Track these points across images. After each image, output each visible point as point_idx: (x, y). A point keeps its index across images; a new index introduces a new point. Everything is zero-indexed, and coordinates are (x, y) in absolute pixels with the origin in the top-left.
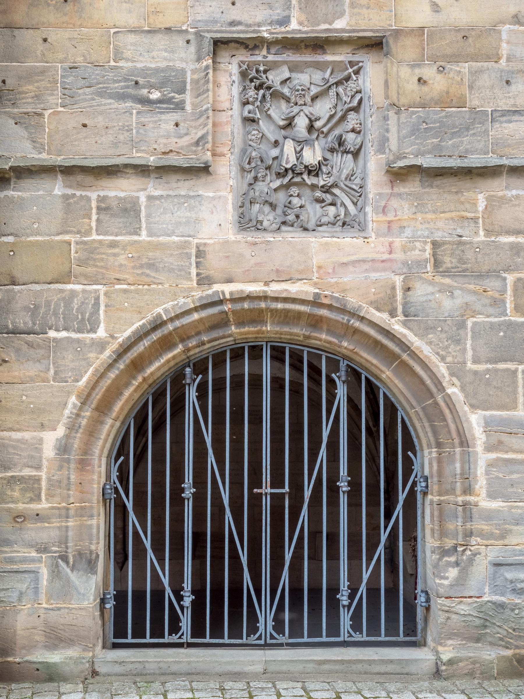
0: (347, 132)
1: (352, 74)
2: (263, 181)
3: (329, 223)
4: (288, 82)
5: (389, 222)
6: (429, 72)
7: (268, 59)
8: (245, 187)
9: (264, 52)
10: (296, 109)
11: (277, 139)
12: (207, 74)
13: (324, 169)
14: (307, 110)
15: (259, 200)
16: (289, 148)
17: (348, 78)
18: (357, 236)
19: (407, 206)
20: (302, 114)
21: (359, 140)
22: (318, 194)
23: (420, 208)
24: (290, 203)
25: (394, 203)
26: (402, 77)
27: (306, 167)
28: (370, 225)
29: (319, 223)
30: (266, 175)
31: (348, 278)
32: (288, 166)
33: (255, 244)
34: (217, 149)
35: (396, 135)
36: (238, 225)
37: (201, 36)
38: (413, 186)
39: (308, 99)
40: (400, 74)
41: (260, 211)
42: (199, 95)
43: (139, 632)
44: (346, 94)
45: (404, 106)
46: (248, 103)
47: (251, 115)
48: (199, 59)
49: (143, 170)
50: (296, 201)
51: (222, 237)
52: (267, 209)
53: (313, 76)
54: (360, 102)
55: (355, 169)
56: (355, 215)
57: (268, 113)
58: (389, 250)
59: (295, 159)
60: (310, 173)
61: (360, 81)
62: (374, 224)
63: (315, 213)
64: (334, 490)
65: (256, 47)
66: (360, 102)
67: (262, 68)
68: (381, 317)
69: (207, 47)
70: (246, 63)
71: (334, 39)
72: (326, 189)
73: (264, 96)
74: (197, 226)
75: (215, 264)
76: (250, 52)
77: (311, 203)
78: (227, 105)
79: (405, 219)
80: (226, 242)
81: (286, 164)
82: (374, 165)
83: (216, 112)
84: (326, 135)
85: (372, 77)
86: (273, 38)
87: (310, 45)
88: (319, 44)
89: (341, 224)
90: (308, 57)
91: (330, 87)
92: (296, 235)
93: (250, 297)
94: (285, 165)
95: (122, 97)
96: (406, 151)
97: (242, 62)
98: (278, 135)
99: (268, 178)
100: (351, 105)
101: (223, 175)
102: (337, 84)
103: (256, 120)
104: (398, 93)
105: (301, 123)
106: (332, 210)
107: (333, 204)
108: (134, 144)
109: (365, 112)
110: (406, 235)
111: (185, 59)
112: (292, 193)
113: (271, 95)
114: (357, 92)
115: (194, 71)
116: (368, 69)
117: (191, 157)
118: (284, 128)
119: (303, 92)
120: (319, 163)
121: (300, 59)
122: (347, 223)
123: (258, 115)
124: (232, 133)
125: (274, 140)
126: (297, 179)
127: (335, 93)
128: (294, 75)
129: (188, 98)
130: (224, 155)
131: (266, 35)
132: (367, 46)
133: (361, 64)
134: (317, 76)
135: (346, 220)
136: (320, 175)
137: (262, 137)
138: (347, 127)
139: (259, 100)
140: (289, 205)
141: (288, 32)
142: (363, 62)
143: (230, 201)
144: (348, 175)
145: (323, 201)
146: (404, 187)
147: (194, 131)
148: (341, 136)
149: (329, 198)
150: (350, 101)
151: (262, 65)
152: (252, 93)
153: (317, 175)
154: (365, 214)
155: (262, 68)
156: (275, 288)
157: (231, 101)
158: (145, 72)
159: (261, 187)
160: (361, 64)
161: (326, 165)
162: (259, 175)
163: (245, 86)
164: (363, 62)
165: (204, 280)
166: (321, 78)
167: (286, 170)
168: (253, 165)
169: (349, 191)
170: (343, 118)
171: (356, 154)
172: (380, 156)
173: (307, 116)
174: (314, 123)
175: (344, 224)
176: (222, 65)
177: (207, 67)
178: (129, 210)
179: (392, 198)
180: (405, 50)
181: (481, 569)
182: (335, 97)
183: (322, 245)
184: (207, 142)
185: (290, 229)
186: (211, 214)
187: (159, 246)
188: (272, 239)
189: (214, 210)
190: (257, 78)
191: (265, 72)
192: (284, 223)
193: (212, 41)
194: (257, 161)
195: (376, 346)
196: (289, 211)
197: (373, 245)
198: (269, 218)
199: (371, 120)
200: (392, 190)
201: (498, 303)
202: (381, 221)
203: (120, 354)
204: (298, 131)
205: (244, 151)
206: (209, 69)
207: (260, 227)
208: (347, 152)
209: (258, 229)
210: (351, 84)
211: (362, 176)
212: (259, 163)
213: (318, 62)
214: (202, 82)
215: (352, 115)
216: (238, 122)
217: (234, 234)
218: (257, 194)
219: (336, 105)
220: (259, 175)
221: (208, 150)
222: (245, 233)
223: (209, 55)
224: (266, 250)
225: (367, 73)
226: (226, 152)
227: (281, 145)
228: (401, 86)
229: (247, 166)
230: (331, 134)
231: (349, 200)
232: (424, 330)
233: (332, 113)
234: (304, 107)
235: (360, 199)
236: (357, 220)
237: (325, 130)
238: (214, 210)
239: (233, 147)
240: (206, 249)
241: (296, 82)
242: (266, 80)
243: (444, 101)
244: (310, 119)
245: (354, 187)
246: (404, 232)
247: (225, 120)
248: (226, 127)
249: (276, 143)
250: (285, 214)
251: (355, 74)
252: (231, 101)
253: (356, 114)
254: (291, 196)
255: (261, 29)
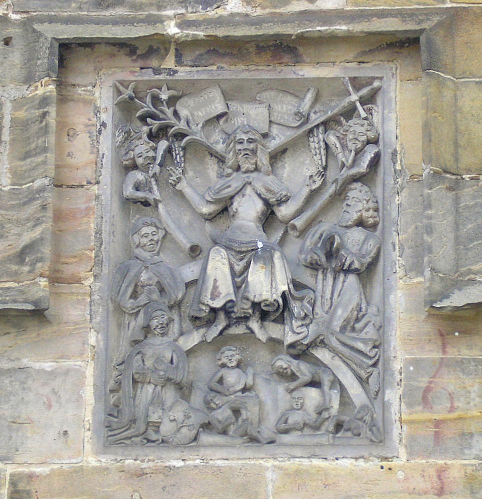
0: (347, 227)
1: (358, 104)
2: (163, 335)
3: (305, 425)
4: (222, 121)
5: (438, 423)
7: (177, 77)
8: (125, 347)
9: (170, 62)
10: (236, 181)
11: (196, 242)
12: (45, 114)
13: (296, 307)
14: (261, 181)
15: (153, 378)
17: (350, 113)
18: (366, 455)
19: (476, 387)
20: (249, 190)
21: (371, 247)
22: (284, 362)
24: (221, 381)
25: (449, 381)
26: (466, 109)
27: (256, 305)
28: (396, 431)
29: (283, 426)
30: (171, 320)
32: (217, 304)
33: (141, 474)
34: (65, 268)
35: (451, 236)
36: (104, 432)
37: (34, 31)
39: (263, 160)
40: (460, 103)
41: (157, 401)
42: (27, 155)
44: (344, 147)
45: (469, 171)
46: (135, 167)
47: (140, 195)
48: (29, 80)
50: (233, 378)
51: (66, 462)
52: (170, 395)
53: (277, 107)
54: (376, 162)
55: (364, 306)
56: (364, 407)
57: (178, 187)
58: (436, 483)
59: (232, 290)
60: (264, 316)
61: (376, 118)
62: (405, 428)
63: (275, 401)
65: (151, 51)
66: (376, 162)
67: (164, 97)
69: (45, 58)
70: (132, 86)
71: (316, 35)
72: (301, 352)
73: (169, 151)
74: (14, 435)
76: (140, 63)
77: (267, 381)
78: (89, 173)
79: (472, 418)
80: (79, 471)
81: (212, 299)
82: (401, 296)
83: (64, 189)
84: (303, 233)
86: (187, 36)
87: (269, 47)
89: (331, 428)
90: (264, 72)
91: (311, 131)
92: (233, 453)
94: (210, 303)
96: (475, 268)
97: (122, 83)
98: (201, 234)
99: (175, 328)
100: (354, 171)
101: (75, 323)
102: (326, 125)
103: (152, 202)
104: (456, 145)
105: (248, 209)
106: (312, 395)
107: (314, 383)
109: (384, 185)
110: (475, 451)
112: (224, 360)
113: (184, 149)
114: (368, 142)
115: (18, 103)
116: (392, 95)
117: (7, 285)
118: (211, 218)
119: (252, 146)
120: (284, 295)
121: (245, 75)
122: (345, 426)
123: (157, 195)
124: (99, 232)
125: (188, 246)
126: (239, 330)
127: (322, 144)
128: (234, 106)
130: (79, 281)
131: (172, 29)
132: (390, 45)
133: (376, 84)
134: (285, 108)
135: (346, 418)
136: (287, 321)
137: (164, 237)
138: (347, 216)
139: (158, 161)
140: (218, 387)
141: (220, 22)
142: (381, 78)
143: (90, 381)
144: (347, 321)
145: (293, 377)
146: (470, 347)
147: (15, 230)
148: (330, 240)
149: (304, 370)
150: (354, 161)
151: (164, 88)
152: (142, 148)
153: (281, 320)
154: (385, 406)
155: (164, 97)
157: (97, 165)
159: (159, 348)
160: (376, 84)
161: (301, 299)
162: (154, 323)
163: (128, 133)
164: (381, 78)
166: (295, 110)
167: (213, 310)
168: (143, 299)
169: (349, 354)
170: (340, 195)
171: (367, 273)
172: (415, 281)
173: (259, 195)
174: (276, 209)
175: (339, 427)
176: (80, 90)
177: (44, 101)
179: (444, 370)
182: (323, 152)
183: (288, 475)
184: (41, 260)
185: (219, 439)
188: (180, 464)
189: (53, 399)
190: (154, 117)
191: (172, 101)
192: (207, 426)
193: (57, 45)
194: (150, 292)
196: (218, 400)
197: (401, 475)
198: (174, 416)
199: (399, 201)
200: (444, 352)
202: (419, 422)
204: (239, 228)
205: (123, 271)
206: (47, 105)
207: (154, 437)
208: (348, 271)
209: (149, 441)
210: (357, 129)
211: (378, 320)
212: (155, 296)
213: (284, 81)
214: (35, 128)
215: (357, 192)
216: (115, 207)
217: (97, 453)
218: (149, 363)
219: (325, 168)
220: (154, 323)
221: (41, 276)
222: (120, 450)
223: (48, 76)
224: (164, 488)
225: (390, 101)
226: (82, 274)
227: (204, 254)
228: (462, 128)
229: (129, 304)
230: (312, 231)
231: (350, 374)
233: (314, 187)
234: (255, 175)
235: (375, 371)
236: (367, 418)
237: (299, 223)
238: (53, 399)
239: (99, 262)
240: (32, 488)
241: (239, 121)
242: (173, 120)
244: (266, 202)
245: (360, 346)
246: (470, 447)
247: (83, 206)
248: (85, 220)
249: (195, 251)
250: (208, 405)
251: (362, 104)
252: (97, 165)
253: (366, 188)
254: (224, 366)
255: (164, 13)
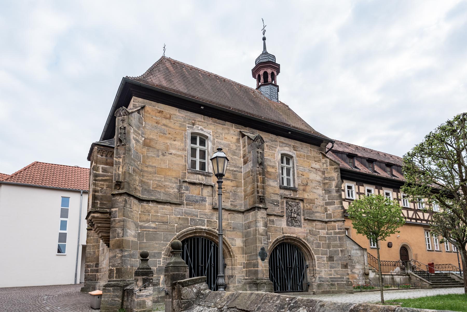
6: (308, 205)
16: (293, 214)
23: (308, 225)
31: (300, 234)
38: (307, 221)
43: (283, 290)
49: (275, 215)
64: (211, 266)
68: (304, 240)
75: (284, 231)
82: (302, 217)
85: (301, 204)
88: (295, 199)
93: (289, 236)
95: (271, 203)
108: (274, 211)
111: (279, 199)
129: (280, 205)
156: (292, 235)
158: (274, 200)
165: (283, 233)
169: (299, 221)
178: (273, 221)
180: (305, 201)
181: (317, 278)
186: (283, 223)
187: (277, 227)
195: (303, 244)
201: (317, 239)
203: (273, 244)
232: (309, 243)
243: (310, 209)
